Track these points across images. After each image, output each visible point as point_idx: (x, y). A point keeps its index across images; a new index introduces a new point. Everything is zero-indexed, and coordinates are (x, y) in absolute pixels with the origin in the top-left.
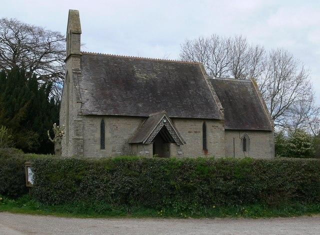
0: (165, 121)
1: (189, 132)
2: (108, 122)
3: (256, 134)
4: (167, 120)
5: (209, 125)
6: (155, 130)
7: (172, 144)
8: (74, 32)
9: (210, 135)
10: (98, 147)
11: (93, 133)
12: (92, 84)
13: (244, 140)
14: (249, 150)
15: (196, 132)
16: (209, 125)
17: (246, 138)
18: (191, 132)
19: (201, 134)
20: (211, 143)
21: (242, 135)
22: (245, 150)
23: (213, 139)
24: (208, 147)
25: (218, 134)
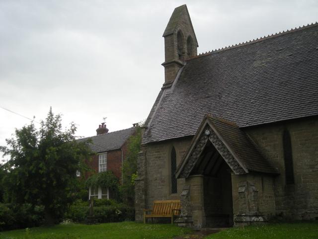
6: (193, 151)
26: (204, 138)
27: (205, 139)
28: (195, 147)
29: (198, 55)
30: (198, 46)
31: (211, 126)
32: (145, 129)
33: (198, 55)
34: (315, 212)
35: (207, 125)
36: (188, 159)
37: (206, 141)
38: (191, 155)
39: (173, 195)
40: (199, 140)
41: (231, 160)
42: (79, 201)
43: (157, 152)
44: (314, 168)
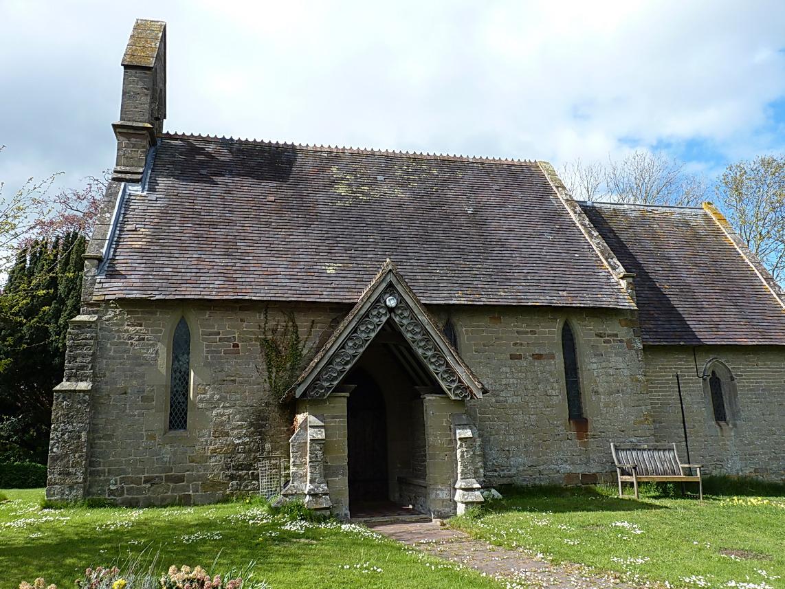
0: (391, 302)
1: (513, 357)
2: (198, 326)
3: (752, 358)
4: (401, 300)
5: (584, 331)
6: (349, 338)
7: (429, 398)
8: (146, 74)
9: (592, 368)
10: (158, 419)
11: (139, 370)
12: (736, 479)
13: (715, 385)
14: (735, 415)
15: (538, 357)
16: (584, 331)
17: (721, 374)
18: (519, 357)
19: (559, 363)
20: (597, 393)
21: (706, 364)
22: (720, 415)
23: (603, 378)
24: (588, 411)
25: (618, 361)
26: (379, 313)
27: (379, 315)
28: (355, 330)
29: (164, 131)
30: (165, 118)
31: (399, 288)
32: (96, 262)
33: (164, 131)
34: (499, 476)
35: (390, 285)
36: (335, 355)
37: (384, 319)
38: (343, 346)
39: (172, 433)
40: (367, 315)
41: (443, 368)
42: (568, 493)
43: (133, 325)
44: (498, 395)
